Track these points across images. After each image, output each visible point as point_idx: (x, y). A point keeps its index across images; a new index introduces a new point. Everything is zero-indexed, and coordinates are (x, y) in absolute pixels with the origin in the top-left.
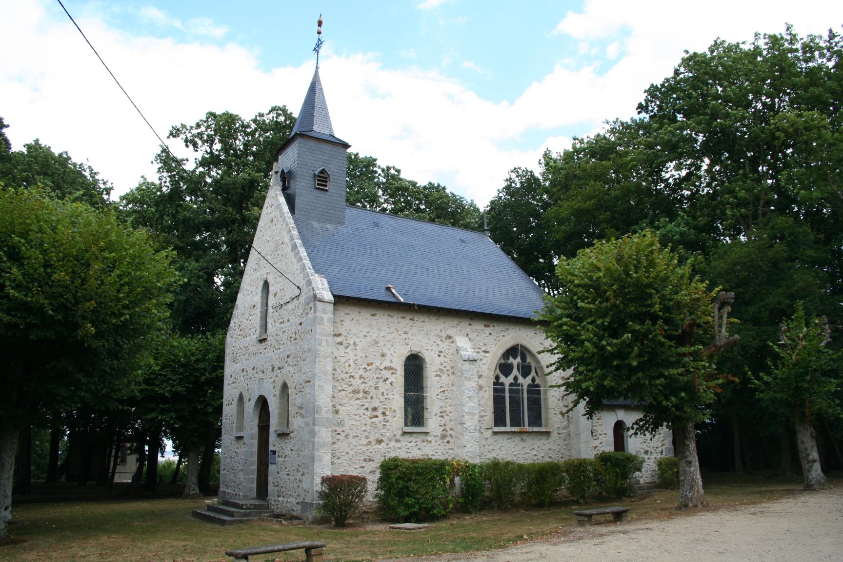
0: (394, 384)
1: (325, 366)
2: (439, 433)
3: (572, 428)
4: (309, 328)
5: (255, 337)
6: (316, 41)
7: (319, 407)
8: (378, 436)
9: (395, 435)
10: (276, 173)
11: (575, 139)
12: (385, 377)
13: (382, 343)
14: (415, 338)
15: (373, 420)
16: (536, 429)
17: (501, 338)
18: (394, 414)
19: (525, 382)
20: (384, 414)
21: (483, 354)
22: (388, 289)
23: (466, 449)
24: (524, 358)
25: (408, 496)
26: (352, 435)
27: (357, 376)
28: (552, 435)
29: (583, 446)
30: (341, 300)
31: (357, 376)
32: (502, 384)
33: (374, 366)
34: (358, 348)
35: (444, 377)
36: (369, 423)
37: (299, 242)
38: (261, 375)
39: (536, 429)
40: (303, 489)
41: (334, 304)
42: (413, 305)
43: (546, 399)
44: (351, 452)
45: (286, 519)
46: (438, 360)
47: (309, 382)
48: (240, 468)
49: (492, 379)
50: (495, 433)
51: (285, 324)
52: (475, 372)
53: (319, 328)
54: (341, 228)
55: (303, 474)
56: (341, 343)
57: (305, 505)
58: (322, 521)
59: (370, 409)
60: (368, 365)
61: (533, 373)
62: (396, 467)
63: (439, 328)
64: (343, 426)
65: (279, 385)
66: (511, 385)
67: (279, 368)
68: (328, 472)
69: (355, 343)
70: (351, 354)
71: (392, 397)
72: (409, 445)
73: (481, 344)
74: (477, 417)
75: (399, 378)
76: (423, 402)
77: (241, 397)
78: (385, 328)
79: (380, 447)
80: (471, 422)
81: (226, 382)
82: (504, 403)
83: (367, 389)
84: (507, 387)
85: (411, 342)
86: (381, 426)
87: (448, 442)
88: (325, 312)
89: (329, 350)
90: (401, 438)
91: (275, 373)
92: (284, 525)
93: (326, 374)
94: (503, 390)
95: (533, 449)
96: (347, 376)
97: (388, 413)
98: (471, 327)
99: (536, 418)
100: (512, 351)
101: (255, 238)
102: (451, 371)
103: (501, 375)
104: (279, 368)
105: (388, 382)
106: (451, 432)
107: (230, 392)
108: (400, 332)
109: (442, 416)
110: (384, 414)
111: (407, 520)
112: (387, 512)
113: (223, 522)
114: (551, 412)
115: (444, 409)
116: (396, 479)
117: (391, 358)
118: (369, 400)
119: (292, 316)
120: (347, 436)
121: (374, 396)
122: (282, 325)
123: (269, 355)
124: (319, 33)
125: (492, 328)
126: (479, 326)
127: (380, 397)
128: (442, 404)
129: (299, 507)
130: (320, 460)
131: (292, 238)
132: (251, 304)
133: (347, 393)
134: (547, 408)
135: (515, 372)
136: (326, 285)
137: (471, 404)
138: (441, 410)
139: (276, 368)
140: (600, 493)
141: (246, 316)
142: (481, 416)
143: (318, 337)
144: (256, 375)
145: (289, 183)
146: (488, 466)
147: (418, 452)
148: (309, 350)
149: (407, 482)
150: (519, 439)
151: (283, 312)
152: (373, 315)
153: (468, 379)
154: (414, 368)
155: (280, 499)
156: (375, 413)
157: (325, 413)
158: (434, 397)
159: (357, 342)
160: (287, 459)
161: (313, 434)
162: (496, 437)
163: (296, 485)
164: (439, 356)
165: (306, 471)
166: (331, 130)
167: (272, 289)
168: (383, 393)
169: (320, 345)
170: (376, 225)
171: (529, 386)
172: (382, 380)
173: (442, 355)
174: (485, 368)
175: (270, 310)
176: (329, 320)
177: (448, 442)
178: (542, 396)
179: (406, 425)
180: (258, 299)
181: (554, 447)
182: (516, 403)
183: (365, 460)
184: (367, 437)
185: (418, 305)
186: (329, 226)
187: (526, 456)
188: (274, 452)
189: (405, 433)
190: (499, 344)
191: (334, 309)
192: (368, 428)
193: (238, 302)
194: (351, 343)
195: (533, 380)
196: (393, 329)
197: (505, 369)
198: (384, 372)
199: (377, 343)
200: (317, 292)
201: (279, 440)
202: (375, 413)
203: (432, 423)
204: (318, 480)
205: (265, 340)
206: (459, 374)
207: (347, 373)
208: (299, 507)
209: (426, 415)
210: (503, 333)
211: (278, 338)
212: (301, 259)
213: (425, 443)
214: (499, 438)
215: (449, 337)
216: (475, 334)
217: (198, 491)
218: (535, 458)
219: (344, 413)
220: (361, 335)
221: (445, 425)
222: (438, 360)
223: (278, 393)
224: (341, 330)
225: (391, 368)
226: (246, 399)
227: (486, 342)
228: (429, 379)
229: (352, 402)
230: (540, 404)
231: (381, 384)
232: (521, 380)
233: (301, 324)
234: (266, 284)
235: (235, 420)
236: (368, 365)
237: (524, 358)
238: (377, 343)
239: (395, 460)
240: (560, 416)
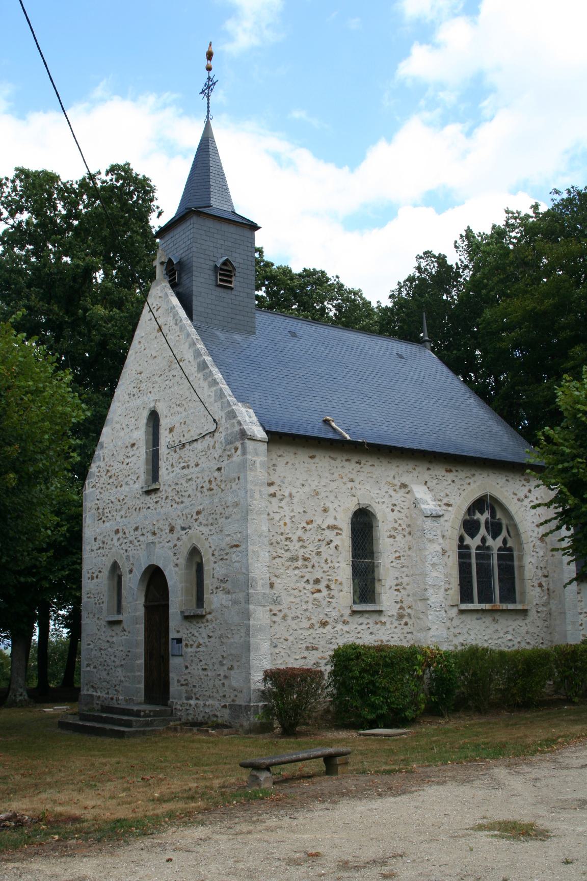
0: (340, 549)
1: (258, 526)
2: (394, 612)
3: (553, 606)
4: (235, 475)
5: (138, 486)
6: (205, 80)
7: (254, 579)
8: (322, 616)
9: (342, 616)
10: (162, 263)
11: (507, 212)
12: (328, 540)
13: (323, 495)
14: (362, 487)
15: (316, 595)
16: (511, 606)
17: (466, 486)
18: (340, 587)
19: (495, 544)
20: (328, 587)
21: (445, 507)
22: (326, 422)
23: (431, 633)
24: (493, 514)
25: (374, 693)
26: (290, 616)
27: (295, 538)
28: (530, 613)
29: (569, 627)
30: (278, 438)
31: (295, 538)
32: (468, 547)
33: (314, 524)
34: (295, 500)
35: (399, 538)
36: (310, 600)
37: (208, 359)
38: (151, 538)
39: (511, 606)
40: (230, 687)
41: (268, 443)
42: (363, 444)
43: (521, 567)
44: (291, 639)
45: (214, 728)
46: (391, 516)
47: (237, 546)
48: (118, 663)
49: (456, 543)
50: (462, 612)
51: (191, 470)
52: (439, 533)
53: (250, 475)
54: (252, 338)
55: (231, 668)
56: (274, 495)
57: (236, 710)
58: (264, 728)
59: (311, 582)
60: (308, 523)
61: (504, 533)
62: (358, 656)
63: (392, 473)
64: (279, 604)
65: (185, 551)
66: (478, 548)
67: (183, 529)
68: (268, 666)
69: (290, 495)
70: (286, 508)
71: (337, 565)
72: (360, 628)
73: (443, 494)
74: (443, 590)
75: (345, 540)
76: (373, 572)
77: (115, 566)
78: (327, 474)
79: (325, 631)
80: (436, 598)
81: (86, 548)
82: (470, 573)
83: (307, 556)
84: (473, 551)
85: (359, 493)
86: (325, 603)
87: (406, 624)
88: (257, 454)
89: (264, 505)
91: (175, 535)
92: (212, 735)
93: (260, 536)
94: (469, 556)
95: (507, 632)
96: (283, 538)
97: (333, 586)
98: (430, 472)
99: (509, 594)
100: (480, 504)
101: (130, 352)
102: (408, 530)
103: (466, 536)
104: (183, 529)
105: (332, 545)
106: (409, 611)
107: (94, 561)
108: (345, 479)
109: (398, 590)
110: (328, 587)
111: (373, 724)
112: (345, 717)
113: (120, 735)
114: (528, 584)
115: (400, 580)
116: (360, 673)
117: (334, 513)
118: (310, 569)
119: (203, 459)
120: (284, 617)
121: (316, 565)
122: (186, 471)
123: (161, 511)
124: (209, 69)
125: (455, 473)
126: (439, 471)
127: (323, 565)
128: (397, 574)
129: (227, 711)
130: (257, 649)
131: (198, 354)
132: (129, 441)
133: (283, 560)
134: (523, 579)
135: (483, 531)
136: (255, 418)
137: (435, 574)
138: (395, 582)
139: (178, 528)
141: (120, 458)
142: (446, 590)
143: (249, 486)
144: (141, 538)
145: (180, 278)
146: (462, 654)
147: (370, 637)
148: (236, 504)
149: (373, 675)
150: (491, 619)
151: (186, 452)
152: (312, 457)
153: (431, 541)
154: (363, 524)
155: (192, 702)
156: (317, 587)
157: (260, 589)
158: (388, 565)
159: (294, 494)
160: (201, 649)
161: (247, 615)
162: (463, 617)
163: (218, 683)
164: (393, 510)
165: (235, 664)
166: (232, 206)
167: (164, 423)
168: (326, 561)
169: (252, 497)
170: (294, 335)
171: (500, 549)
172: (325, 543)
173: (396, 509)
174: (448, 525)
175: (163, 450)
176: (262, 464)
177: (406, 624)
178: (516, 563)
179: (355, 602)
180: (140, 435)
181: (532, 630)
182: (485, 572)
183: (307, 648)
184: (309, 619)
185: (369, 444)
186: (237, 337)
187: (499, 641)
188: (179, 641)
189: (354, 613)
190: (464, 494)
191: (268, 450)
192: (310, 606)
193: (103, 439)
194: (287, 494)
195: (505, 541)
196: (336, 476)
197: (470, 527)
198: (327, 532)
199: (317, 494)
200: (245, 427)
201: (187, 624)
202: (317, 587)
203: (387, 599)
204: (257, 677)
205: (156, 490)
206: (419, 534)
207: (282, 534)
208: (227, 711)
209: (378, 588)
210: (468, 481)
211: (178, 488)
212: (215, 382)
213: (379, 626)
214: (467, 618)
215: (404, 486)
216: (435, 482)
217: (26, 697)
218: (510, 644)
219: (281, 586)
220: (298, 484)
221: (402, 601)
222: (391, 516)
223: (182, 561)
224: (274, 478)
225: (334, 527)
226: (124, 570)
227: (447, 491)
228: (381, 541)
229: (290, 572)
230: (513, 573)
231: (323, 549)
232: (490, 542)
233: (219, 469)
234: (154, 418)
235: (105, 599)
236: (308, 523)
237: (493, 514)
238: (317, 494)
239: (354, 647)
240: (539, 589)
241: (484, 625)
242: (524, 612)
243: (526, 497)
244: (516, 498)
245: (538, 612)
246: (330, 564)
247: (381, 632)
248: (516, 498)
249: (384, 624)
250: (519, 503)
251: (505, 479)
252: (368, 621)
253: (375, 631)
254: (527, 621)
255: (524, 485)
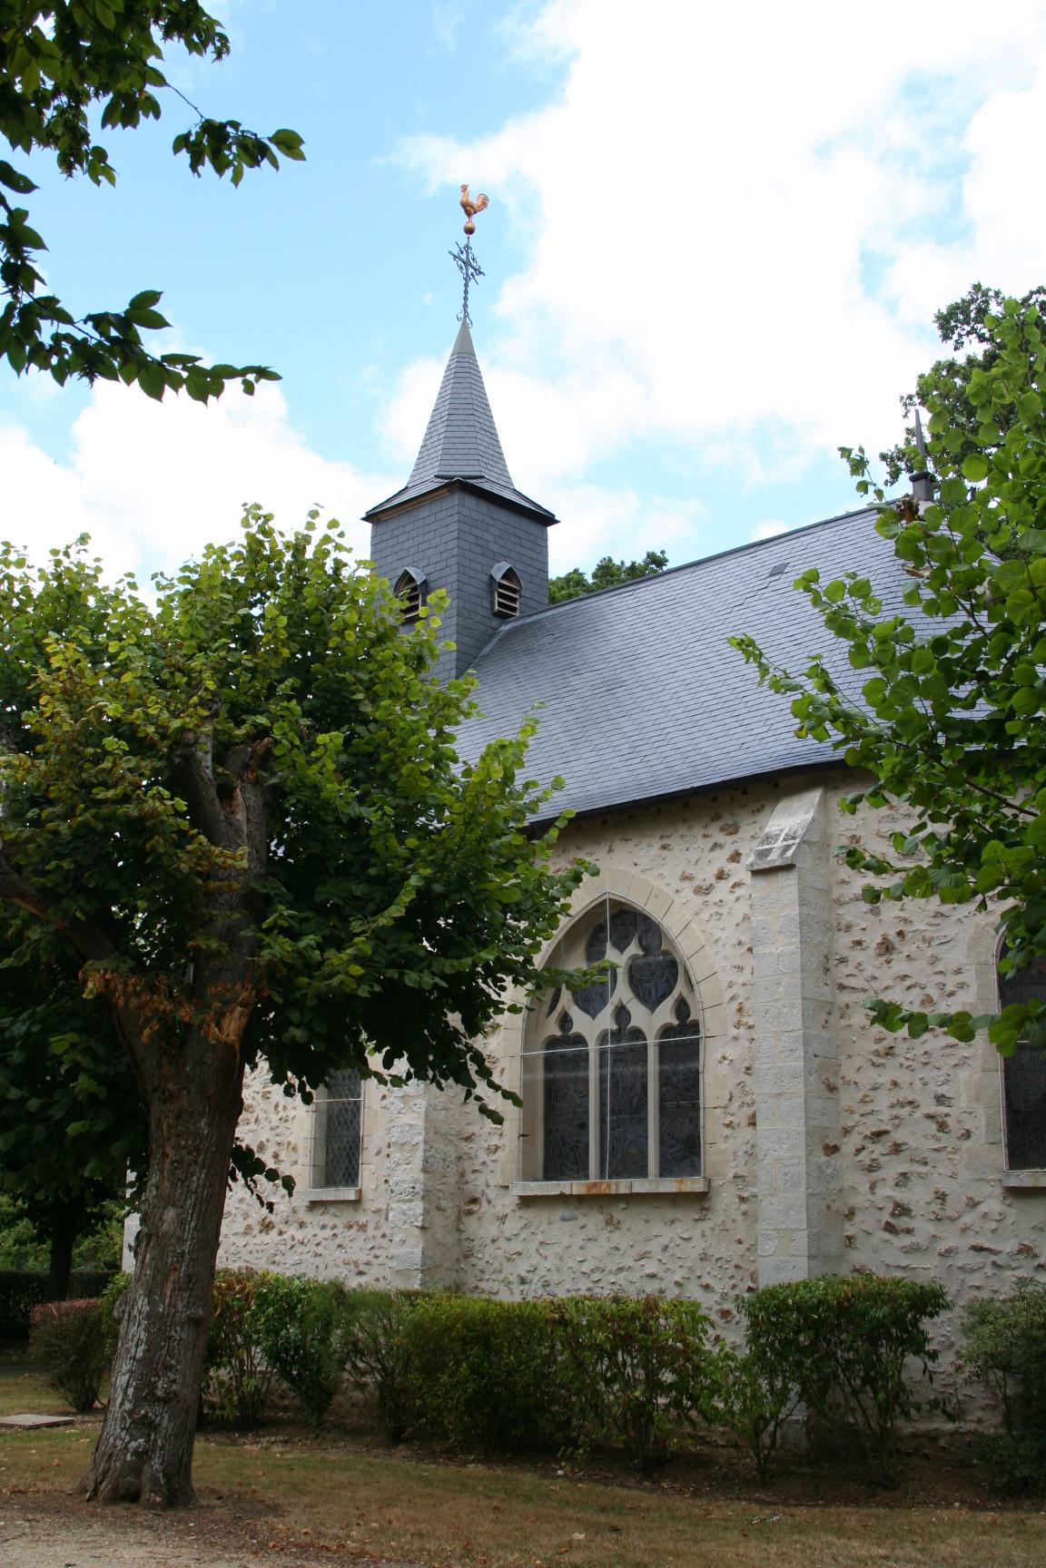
16: (623, 1186)
18: (294, 1156)
19: (651, 1021)
39: (623, 1186)
66: (667, 1031)
72: (322, 1234)
84: (652, 1041)
90: (307, 1218)
99: (684, 1149)
112: (402, 1422)
140: (252, 1374)
162: (530, 1214)
168: (277, 1106)
187: (621, 1278)
213: (353, 1231)
232: (640, 1016)
241: (582, 1235)
242: (700, 1200)
243: (721, 876)
244: (688, 887)
245: (743, 1200)
246: (282, 1114)
247: (356, 1245)
248: (688, 887)
249: (363, 1227)
250: (700, 899)
251: (657, 844)
252: (336, 1221)
253: (346, 1243)
254: (706, 1226)
255: (716, 846)
